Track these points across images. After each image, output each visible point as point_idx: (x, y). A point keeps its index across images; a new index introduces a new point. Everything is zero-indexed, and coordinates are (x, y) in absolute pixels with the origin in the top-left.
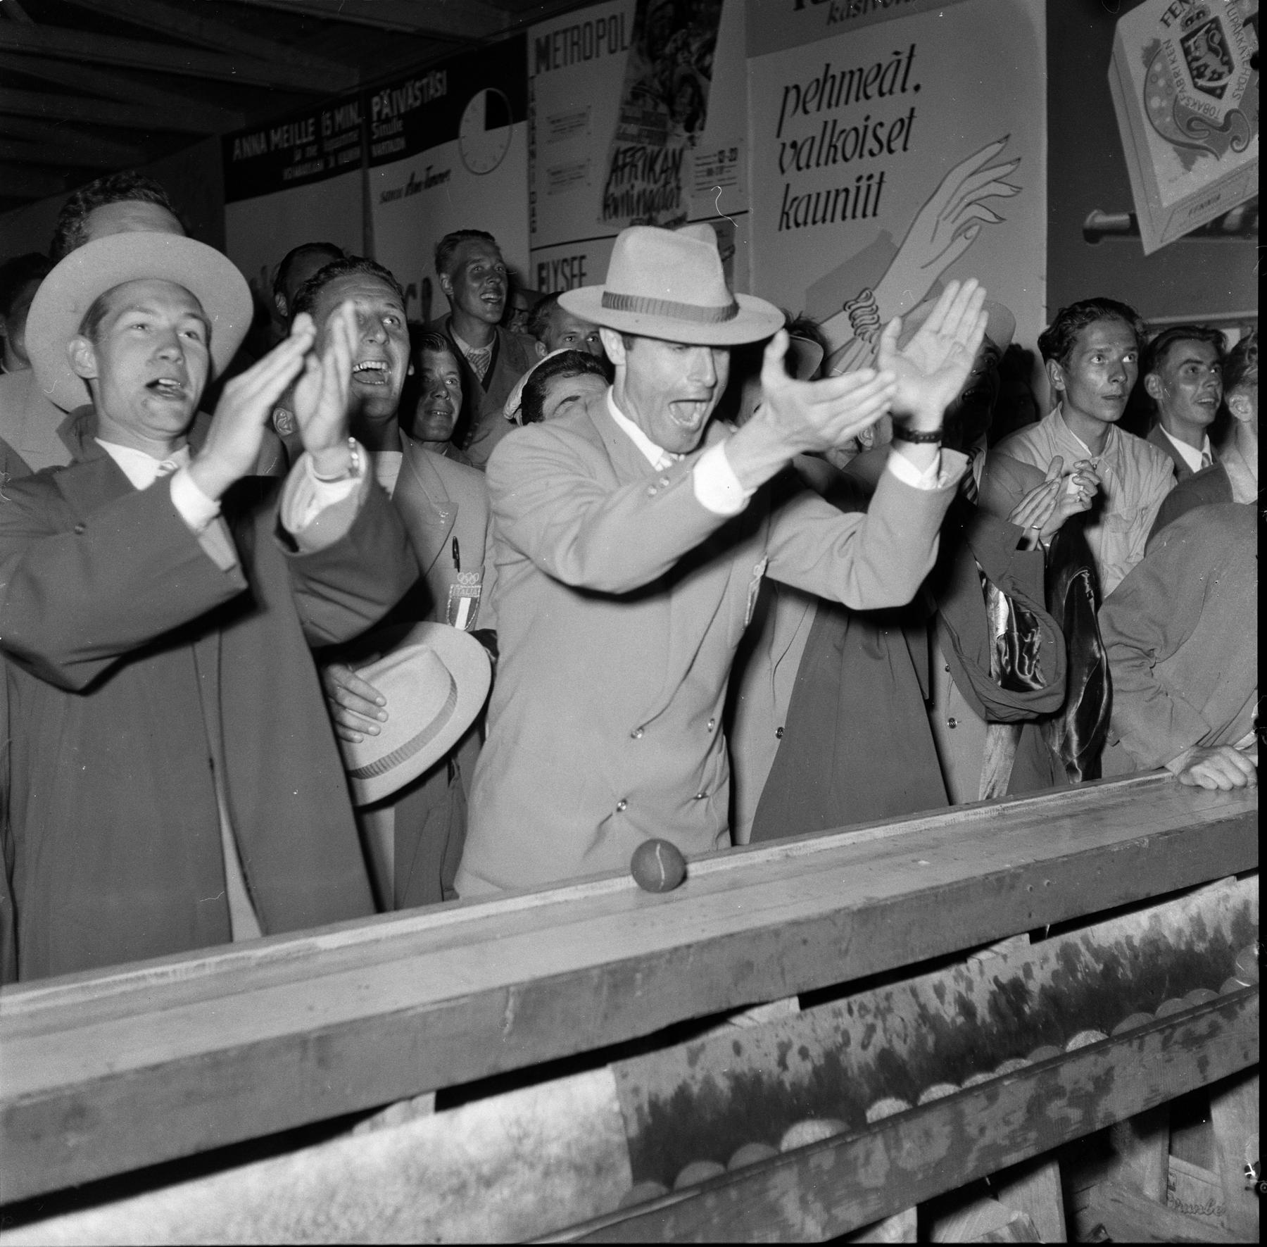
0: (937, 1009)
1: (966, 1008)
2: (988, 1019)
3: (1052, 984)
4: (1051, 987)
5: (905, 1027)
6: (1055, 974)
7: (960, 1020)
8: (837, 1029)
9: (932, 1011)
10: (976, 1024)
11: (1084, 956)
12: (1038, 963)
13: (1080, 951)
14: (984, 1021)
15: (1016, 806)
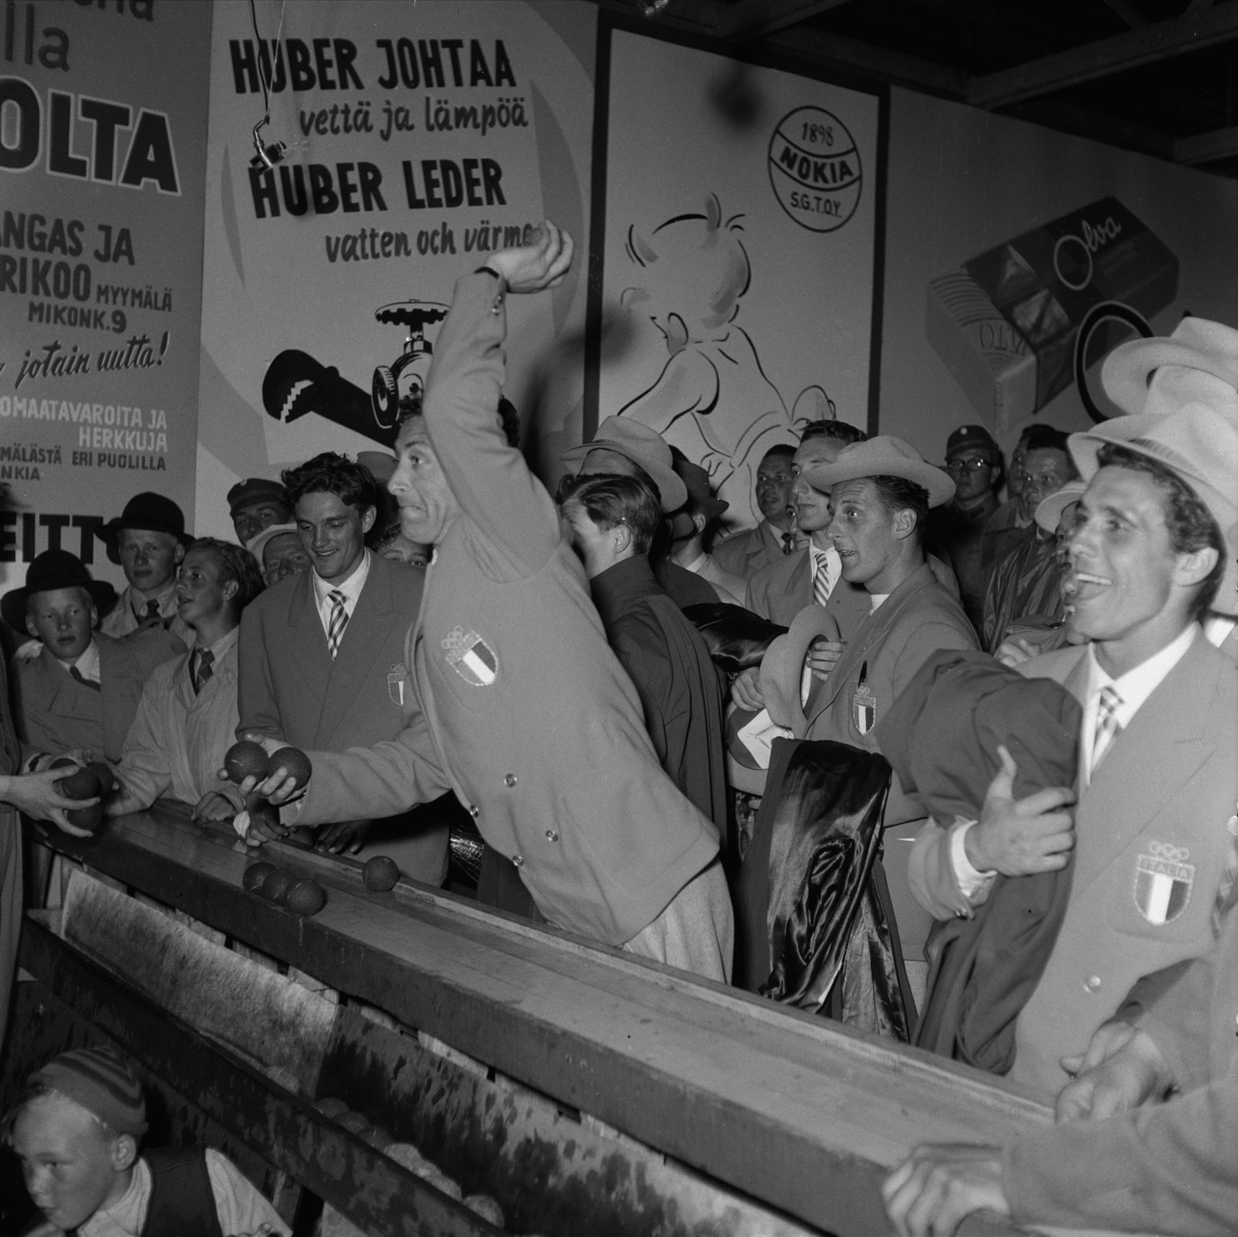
0: (481, 1115)
1: (500, 1134)
2: (511, 1157)
3: (584, 1180)
4: (581, 1182)
5: (458, 1109)
6: (592, 1174)
7: (490, 1137)
8: (428, 1074)
9: (477, 1113)
10: (498, 1151)
11: (630, 1182)
12: (584, 1149)
13: (628, 1174)
14: (506, 1155)
15: (921, 1070)
